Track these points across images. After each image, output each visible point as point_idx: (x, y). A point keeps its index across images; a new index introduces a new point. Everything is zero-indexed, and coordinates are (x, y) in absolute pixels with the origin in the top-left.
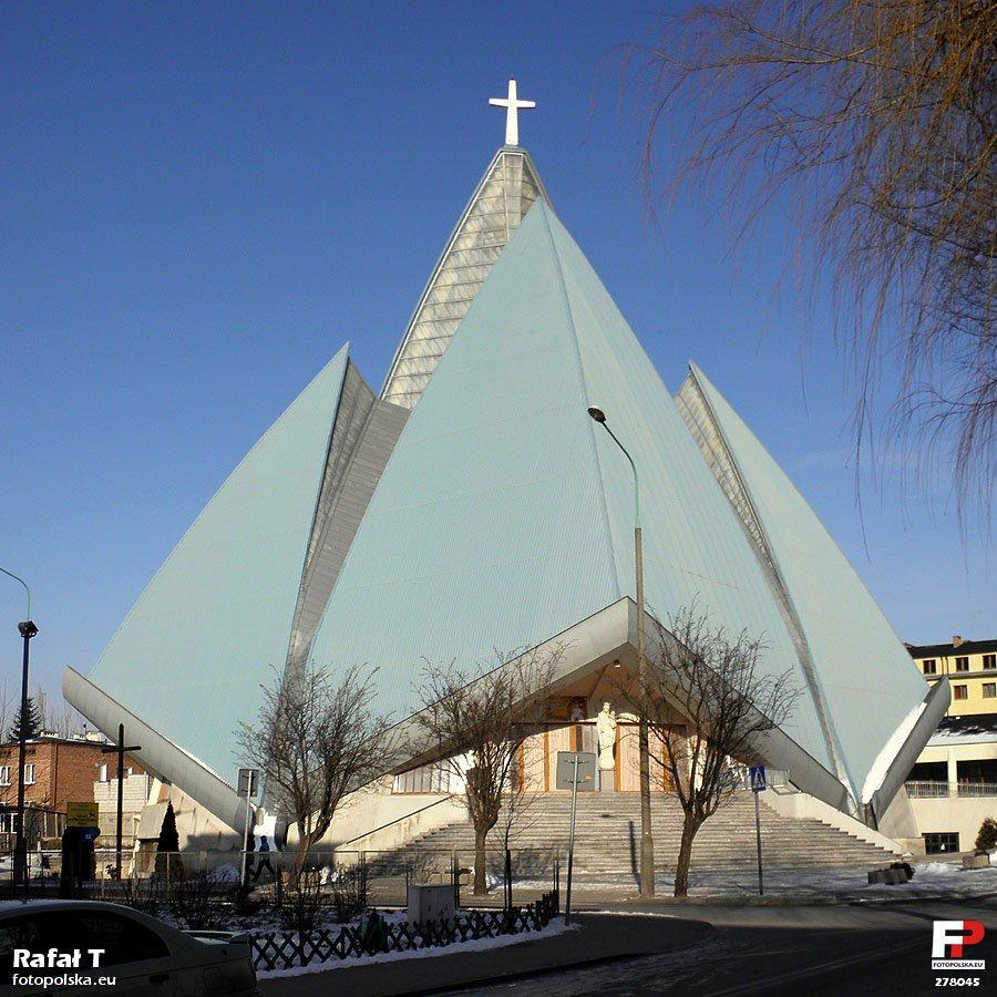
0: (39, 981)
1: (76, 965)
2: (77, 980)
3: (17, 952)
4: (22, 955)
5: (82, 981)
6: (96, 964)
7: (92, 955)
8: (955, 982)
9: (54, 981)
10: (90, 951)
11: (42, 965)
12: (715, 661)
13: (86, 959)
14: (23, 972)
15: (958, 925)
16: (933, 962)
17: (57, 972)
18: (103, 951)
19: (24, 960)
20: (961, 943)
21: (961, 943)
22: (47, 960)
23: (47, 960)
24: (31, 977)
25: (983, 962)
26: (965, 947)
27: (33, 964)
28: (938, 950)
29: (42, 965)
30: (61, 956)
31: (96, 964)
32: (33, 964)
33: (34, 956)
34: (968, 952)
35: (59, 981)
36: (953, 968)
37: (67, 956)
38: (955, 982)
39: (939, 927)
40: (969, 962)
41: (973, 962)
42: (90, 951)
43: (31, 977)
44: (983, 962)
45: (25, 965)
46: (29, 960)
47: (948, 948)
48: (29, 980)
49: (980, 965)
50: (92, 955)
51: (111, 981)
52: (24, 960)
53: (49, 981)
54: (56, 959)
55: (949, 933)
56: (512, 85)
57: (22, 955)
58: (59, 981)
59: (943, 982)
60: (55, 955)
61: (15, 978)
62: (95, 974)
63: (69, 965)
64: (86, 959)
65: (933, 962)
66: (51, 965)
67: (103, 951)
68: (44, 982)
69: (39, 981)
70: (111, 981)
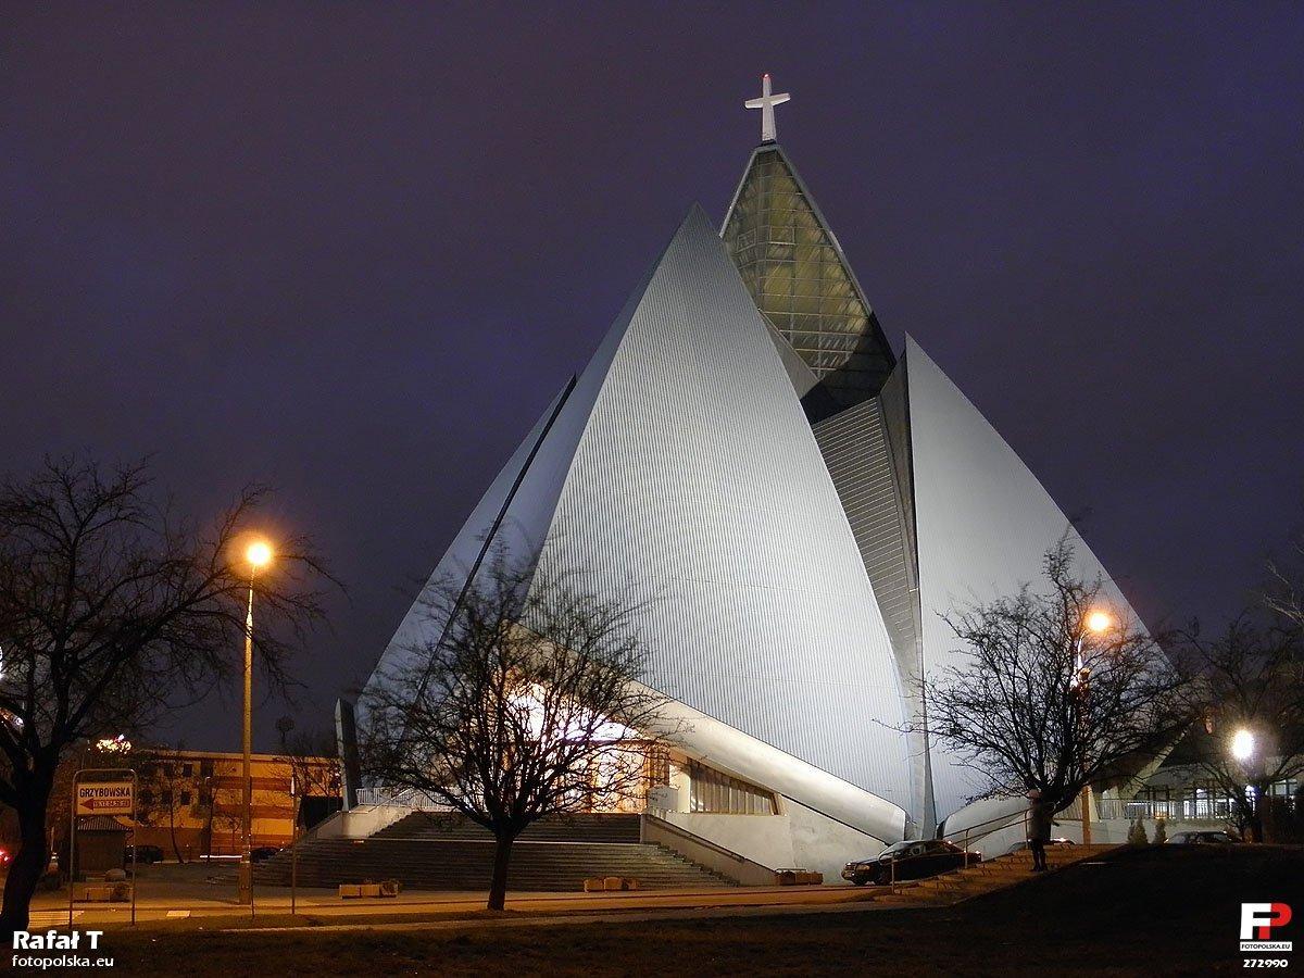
0: (38, 962)
1: (75, 947)
2: (76, 962)
3: (17, 934)
4: (21, 937)
5: (80, 962)
6: (94, 946)
7: (90, 937)
8: (1270, 963)
9: (53, 962)
10: (88, 933)
11: (41, 947)
12: (607, 644)
13: (84, 941)
14: (22, 953)
15: (1266, 908)
16: (1242, 943)
17: (56, 953)
18: (101, 933)
19: (23, 941)
20: (1269, 925)
21: (1269, 925)
22: (46, 942)
23: (46, 942)
24: (30, 959)
25: (1290, 943)
26: (1272, 928)
27: (33, 946)
28: (1246, 932)
29: (41, 947)
30: (60, 937)
31: (94, 946)
32: (33, 946)
33: (34, 938)
34: (1276, 934)
35: (58, 962)
36: (1261, 949)
37: (66, 938)
38: (1270, 963)
39: (1248, 909)
40: (1276, 943)
41: (1281, 944)
42: (88, 933)
43: (30, 959)
44: (1290, 943)
45: (25, 946)
46: (28, 942)
47: (1256, 930)
48: (28, 962)
49: (1287, 946)
50: (90, 937)
51: (109, 962)
52: (23, 941)
53: (48, 962)
54: (55, 941)
55: (1257, 915)
56: (749, 105)
57: (21, 937)
58: (58, 962)
59: (1258, 963)
60: (54, 937)
61: (14, 959)
62: (93, 955)
63: (67, 947)
64: (84, 941)
65: (1242, 943)
66: (50, 946)
67: (101, 933)
68: (43, 963)
69: (38, 962)
70: (109, 962)
